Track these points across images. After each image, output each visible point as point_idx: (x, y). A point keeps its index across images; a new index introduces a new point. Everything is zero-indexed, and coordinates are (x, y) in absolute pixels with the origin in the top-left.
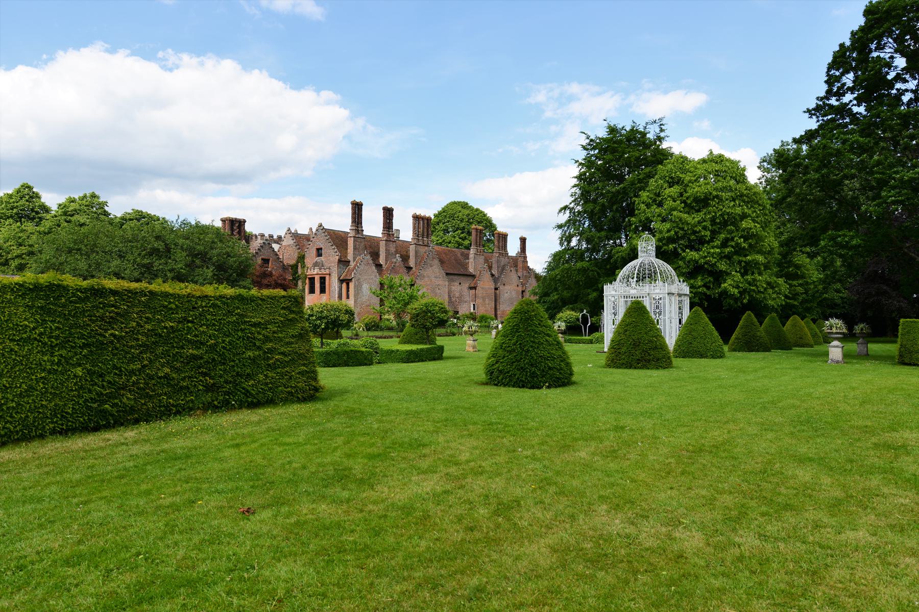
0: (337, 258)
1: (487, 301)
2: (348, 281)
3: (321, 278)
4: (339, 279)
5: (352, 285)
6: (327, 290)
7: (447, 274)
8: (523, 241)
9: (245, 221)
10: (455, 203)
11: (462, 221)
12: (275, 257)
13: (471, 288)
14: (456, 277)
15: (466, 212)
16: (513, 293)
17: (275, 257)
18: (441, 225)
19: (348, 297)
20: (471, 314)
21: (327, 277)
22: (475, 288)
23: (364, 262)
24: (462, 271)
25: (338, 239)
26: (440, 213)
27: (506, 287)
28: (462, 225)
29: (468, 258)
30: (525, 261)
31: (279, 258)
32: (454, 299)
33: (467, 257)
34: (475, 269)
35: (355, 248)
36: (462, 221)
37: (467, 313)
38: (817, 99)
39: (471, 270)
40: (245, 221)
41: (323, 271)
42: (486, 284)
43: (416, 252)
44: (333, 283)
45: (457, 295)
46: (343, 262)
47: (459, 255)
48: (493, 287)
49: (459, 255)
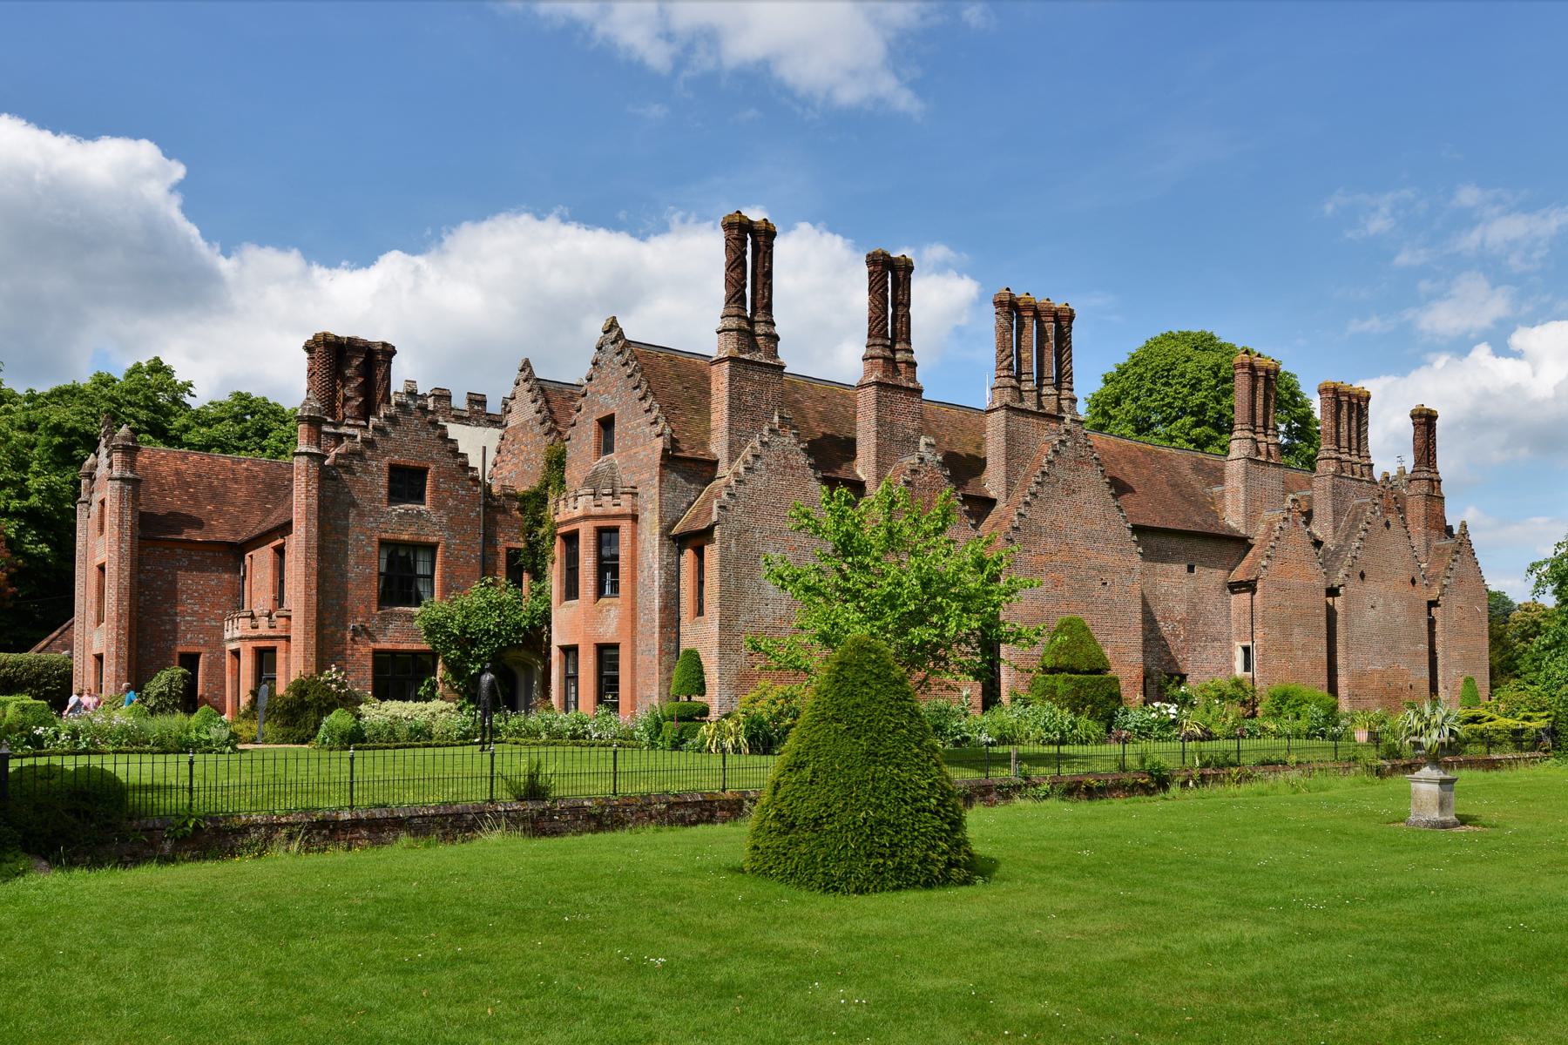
0: (659, 444)
1: (1298, 637)
2: (696, 540)
3: (600, 531)
4: (666, 533)
5: (712, 553)
6: (624, 581)
7: (1137, 530)
8: (1425, 421)
9: (389, 352)
10: (1171, 337)
11: (1195, 386)
12: (452, 464)
13: (1235, 587)
14: (1173, 543)
15: (1209, 359)
16: (1397, 608)
17: (452, 464)
18: (1127, 404)
19: (700, 611)
20: (1238, 684)
21: (625, 526)
22: (1249, 586)
23: (770, 457)
24: (1196, 522)
25: (664, 376)
26: (1122, 371)
27: (1370, 585)
28: (1197, 398)
29: (1220, 481)
30: (1434, 497)
31: (465, 467)
32: (1165, 628)
33: (1217, 476)
34: (1251, 516)
35: (736, 407)
36: (1195, 386)
37: (1222, 681)
38: (1464, 525)
39: (1233, 519)
40: (389, 352)
41: (608, 506)
42: (1287, 573)
43: (1011, 439)
44: (646, 550)
45: (1180, 610)
46: (686, 465)
47: (1186, 469)
48: (1321, 584)
49: (1186, 469)
